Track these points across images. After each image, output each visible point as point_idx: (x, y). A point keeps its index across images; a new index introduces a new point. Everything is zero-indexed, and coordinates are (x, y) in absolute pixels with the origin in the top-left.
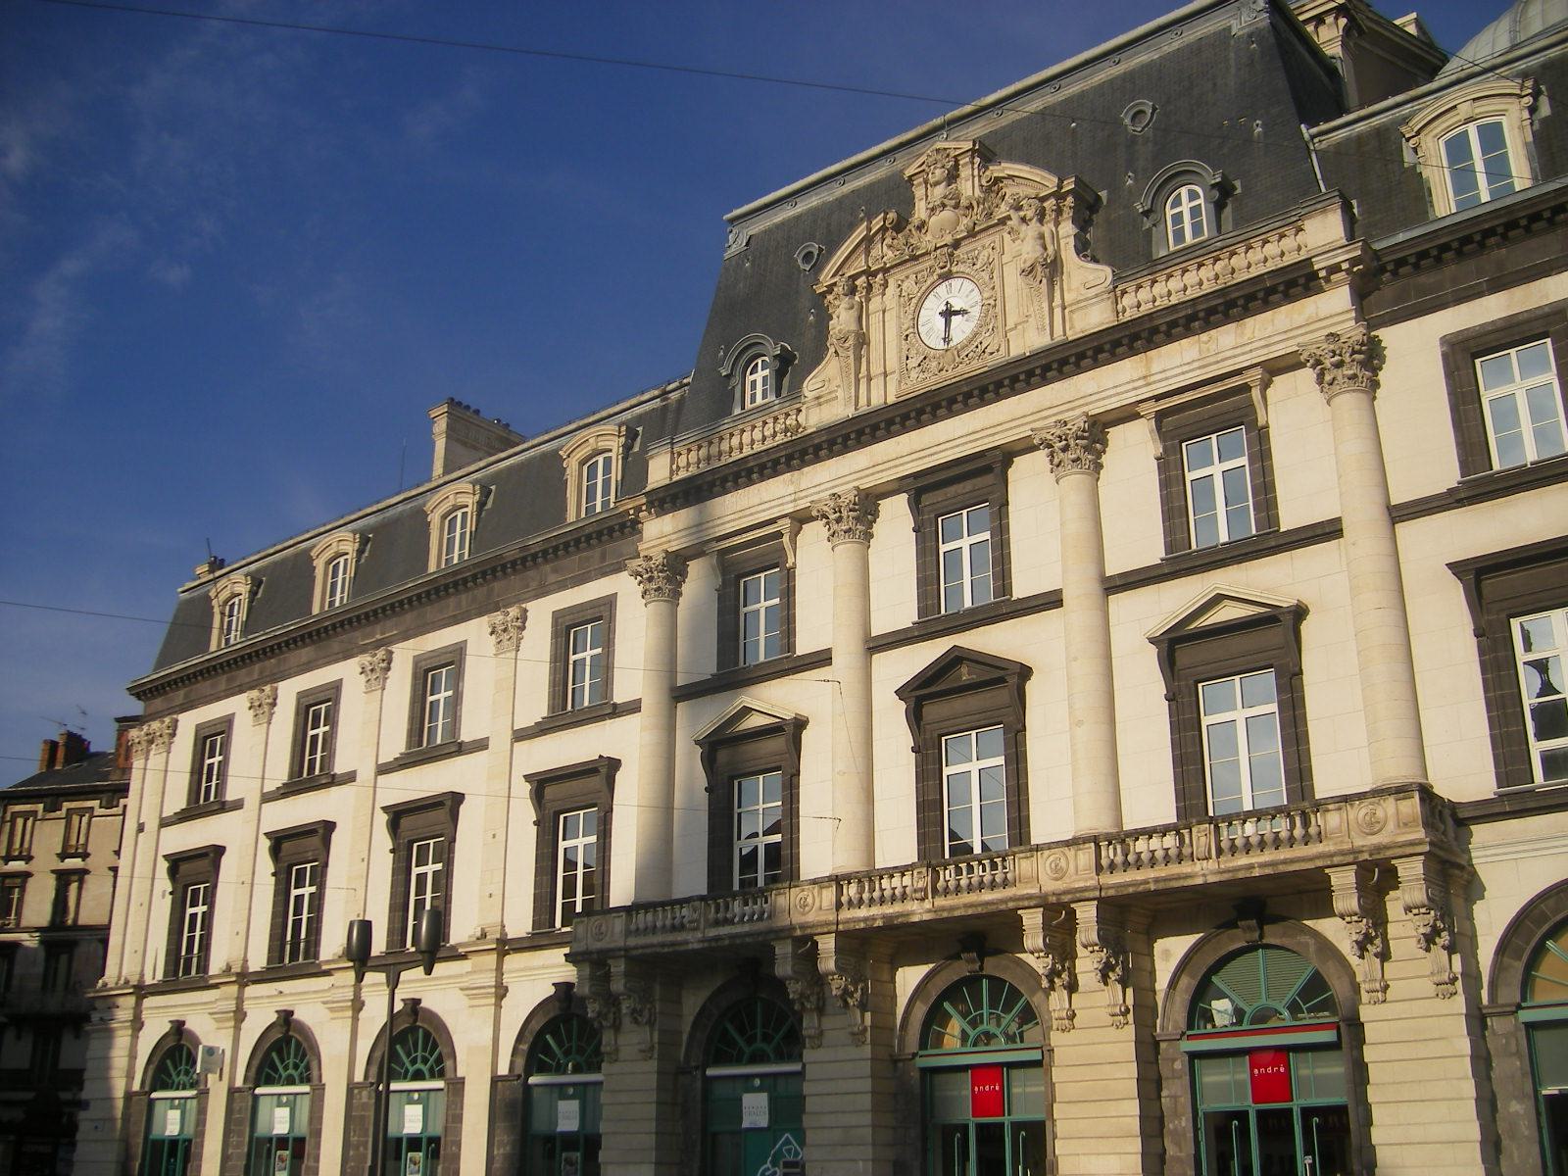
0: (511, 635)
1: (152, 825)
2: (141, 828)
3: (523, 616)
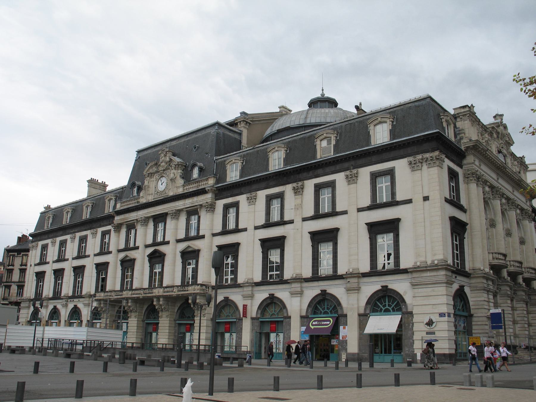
0: (252, 201)
1: (33, 265)
2: (31, 266)
3: (97, 232)
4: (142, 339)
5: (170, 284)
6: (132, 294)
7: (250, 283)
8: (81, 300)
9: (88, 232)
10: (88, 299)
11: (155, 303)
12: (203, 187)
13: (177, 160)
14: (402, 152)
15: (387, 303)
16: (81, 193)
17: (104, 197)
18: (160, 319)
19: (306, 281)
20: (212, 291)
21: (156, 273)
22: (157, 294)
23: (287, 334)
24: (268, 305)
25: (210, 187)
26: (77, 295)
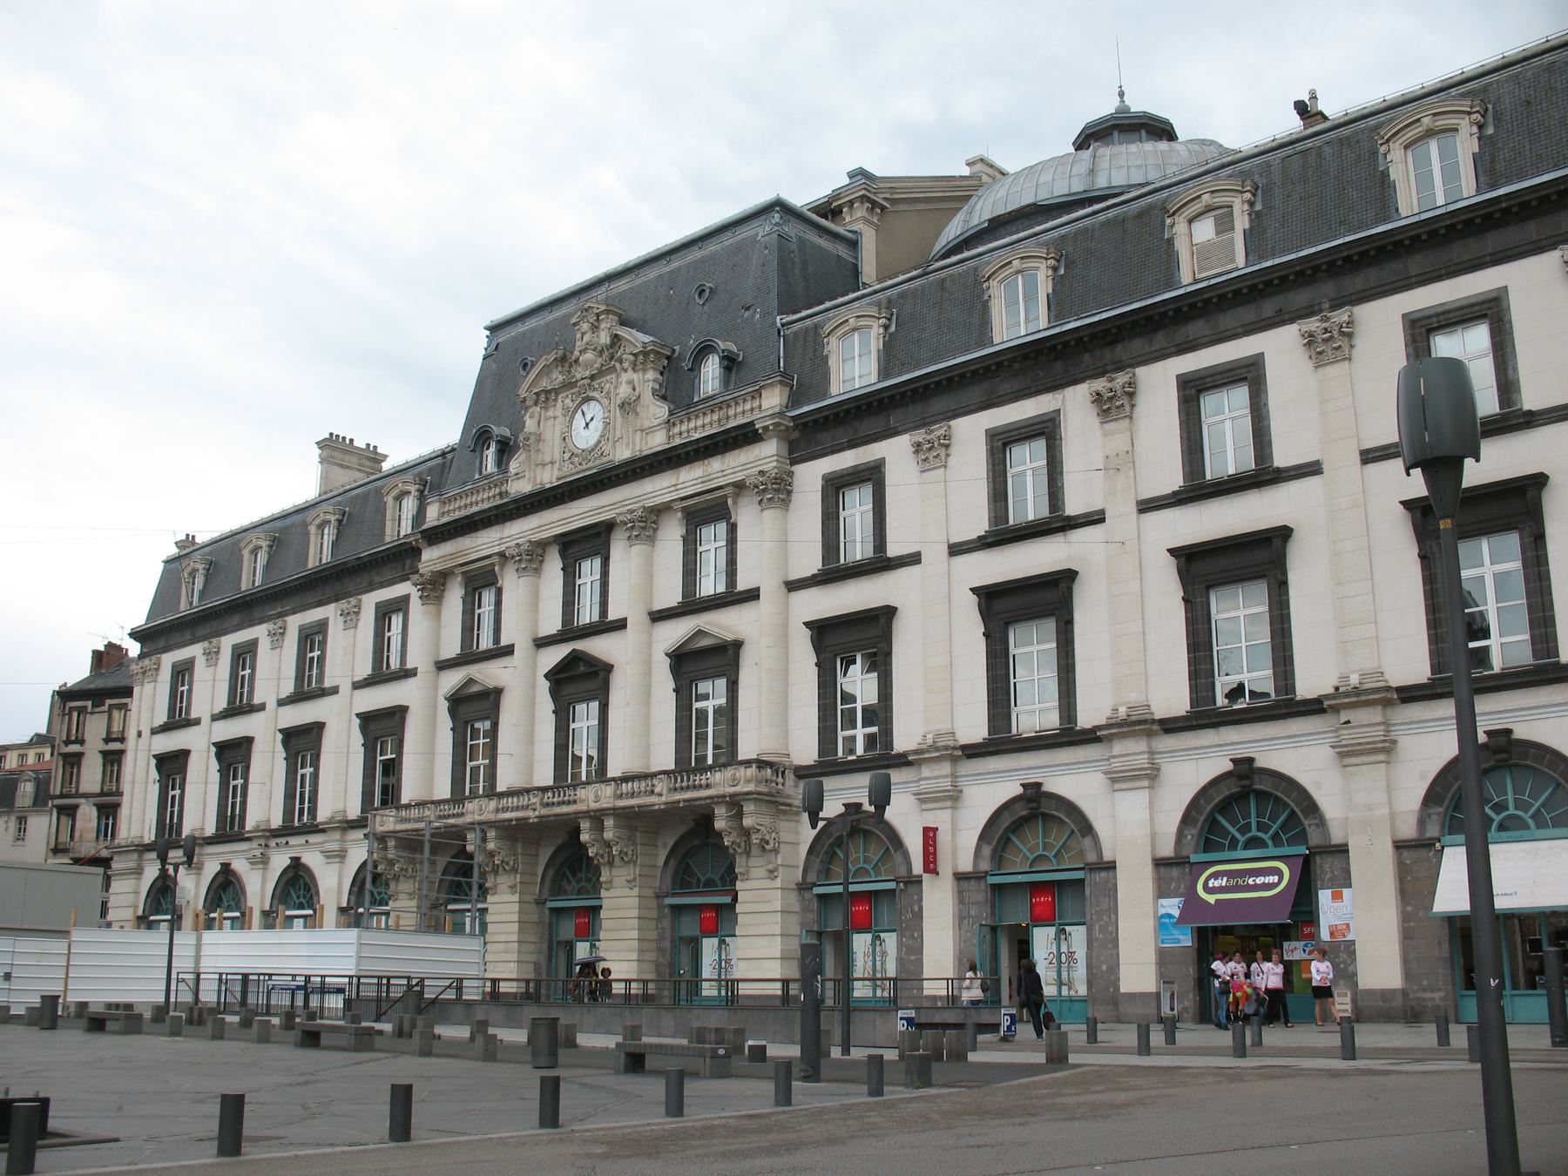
1: (146, 733)
2: (139, 734)
4: (537, 965)
5: (636, 767)
6: (497, 810)
7: (946, 748)
8: (314, 838)
9: (329, 612)
10: (337, 835)
11: (584, 837)
12: (741, 421)
13: (637, 339)
14: (1532, 230)
16: (297, 482)
17: (378, 491)
18: (603, 893)
19: (1168, 731)
20: (796, 786)
21: (702, 714)
22: (593, 806)
23: (1103, 929)
24: (1017, 826)
25: (772, 416)
26: (299, 821)
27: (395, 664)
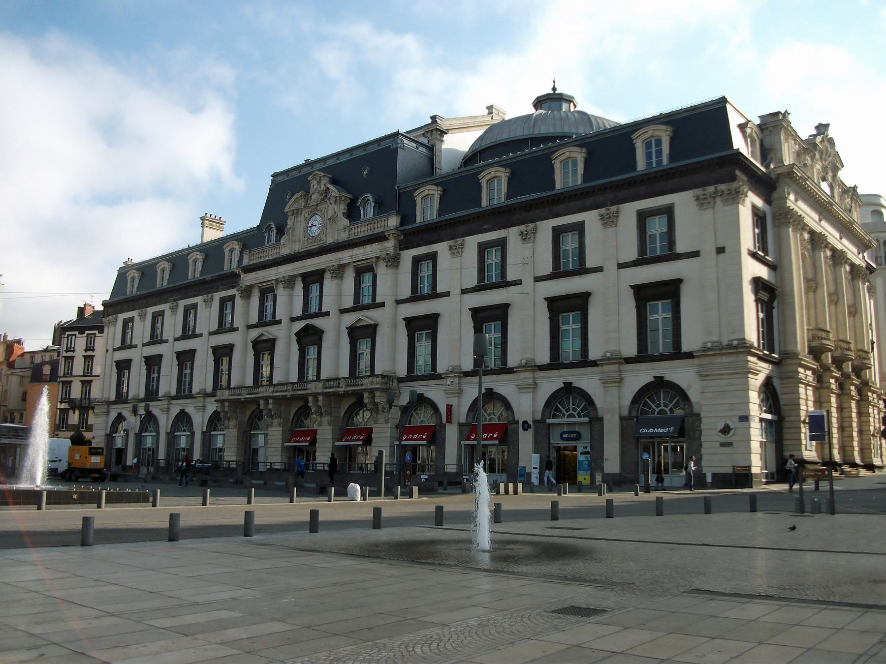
0: (457, 251)
1: (110, 350)
3: (212, 298)
5: (283, 380)
9: (198, 300)
11: (262, 407)
12: (380, 230)
15: (571, 406)
19: (541, 370)
22: (314, 391)
27: (228, 325)
